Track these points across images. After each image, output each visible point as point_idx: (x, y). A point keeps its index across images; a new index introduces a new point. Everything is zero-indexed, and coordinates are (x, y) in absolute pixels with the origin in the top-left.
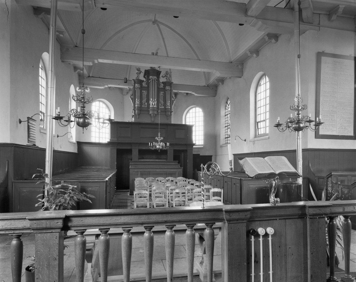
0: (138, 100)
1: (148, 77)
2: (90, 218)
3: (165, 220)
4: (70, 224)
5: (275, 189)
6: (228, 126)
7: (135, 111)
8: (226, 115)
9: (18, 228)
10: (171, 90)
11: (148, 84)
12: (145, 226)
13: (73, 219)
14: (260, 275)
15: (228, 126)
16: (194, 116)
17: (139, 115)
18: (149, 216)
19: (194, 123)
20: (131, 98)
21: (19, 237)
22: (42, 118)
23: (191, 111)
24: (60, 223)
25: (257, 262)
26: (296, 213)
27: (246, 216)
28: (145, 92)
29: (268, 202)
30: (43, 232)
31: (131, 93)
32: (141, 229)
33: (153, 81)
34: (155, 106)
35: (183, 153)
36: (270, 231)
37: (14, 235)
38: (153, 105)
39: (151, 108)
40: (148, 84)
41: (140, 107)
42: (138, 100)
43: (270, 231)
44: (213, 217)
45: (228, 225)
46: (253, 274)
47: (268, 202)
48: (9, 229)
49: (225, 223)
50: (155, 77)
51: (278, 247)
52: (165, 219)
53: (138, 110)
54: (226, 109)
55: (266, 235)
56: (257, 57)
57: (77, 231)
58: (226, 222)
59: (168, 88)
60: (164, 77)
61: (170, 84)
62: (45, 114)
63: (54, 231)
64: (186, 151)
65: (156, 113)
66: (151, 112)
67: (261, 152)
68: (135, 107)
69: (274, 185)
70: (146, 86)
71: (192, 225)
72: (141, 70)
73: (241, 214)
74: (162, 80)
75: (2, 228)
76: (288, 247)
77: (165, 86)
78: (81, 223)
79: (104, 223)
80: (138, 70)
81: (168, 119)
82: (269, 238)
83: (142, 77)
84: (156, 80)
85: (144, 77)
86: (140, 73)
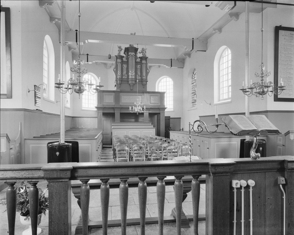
0: (120, 73)
1: (128, 53)
2: (93, 169)
3: (157, 172)
4: (76, 175)
5: (256, 145)
6: (195, 92)
7: (117, 81)
8: (192, 84)
9: (34, 177)
10: (146, 64)
11: (128, 59)
12: (139, 177)
13: (79, 170)
14: (241, 223)
15: (195, 92)
16: (165, 84)
17: (120, 84)
18: (143, 168)
19: (165, 91)
20: (114, 71)
21: (12, 185)
22: (45, 88)
23: (162, 81)
24: (69, 174)
25: (239, 210)
26: (276, 167)
27: (230, 169)
28: (125, 66)
29: (249, 156)
30: (54, 181)
31: (114, 67)
32: (136, 179)
33: (132, 56)
34: (133, 77)
35: (157, 115)
36: (252, 183)
37: (31, 183)
38: (131, 76)
39: (130, 79)
40: (128, 59)
41: (121, 78)
42: (120, 73)
43: (252, 183)
44: (200, 170)
45: (214, 177)
46: (235, 221)
47: (249, 156)
48: (27, 178)
49: (210, 175)
50: (134, 53)
51: (258, 197)
52: (157, 172)
53: (119, 80)
54: (192, 78)
55: (248, 187)
56: (220, 33)
57: (82, 181)
58: (211, 174)
59: (144, 62)
60: (140, 53)
61: (145, 58)
62: (47, 85)
63: (63, 180)
64: (160, 113)
65: (134, 82)
66: (130, 82)
67: (270, 111)
68: (117, 78)
69: (255, 141)
70: (126, 61)
71: (180, 177)
72: (122, 48)
73: (225, 167)
74: (139, 55)
75: (22, 177)
76: (267, 197)
77: (141, 61)
78: (85, 174)
79: (104, 174)
80: (119, 48)
81: (144, 88)
82: (250, 189)
83: (122, 54)
84: (134, 56)
85: (124, 53)
86: (121, 50)
